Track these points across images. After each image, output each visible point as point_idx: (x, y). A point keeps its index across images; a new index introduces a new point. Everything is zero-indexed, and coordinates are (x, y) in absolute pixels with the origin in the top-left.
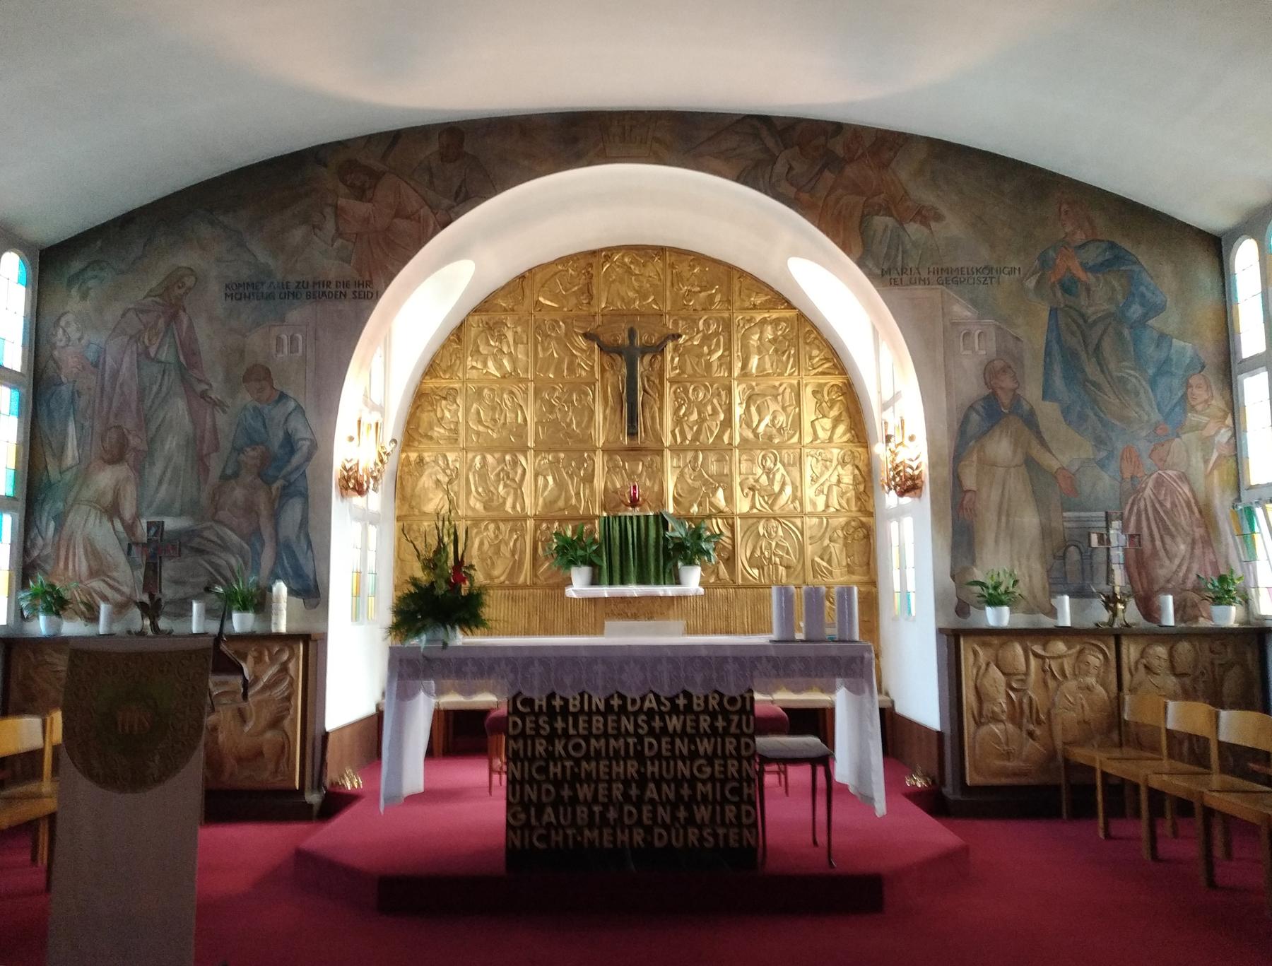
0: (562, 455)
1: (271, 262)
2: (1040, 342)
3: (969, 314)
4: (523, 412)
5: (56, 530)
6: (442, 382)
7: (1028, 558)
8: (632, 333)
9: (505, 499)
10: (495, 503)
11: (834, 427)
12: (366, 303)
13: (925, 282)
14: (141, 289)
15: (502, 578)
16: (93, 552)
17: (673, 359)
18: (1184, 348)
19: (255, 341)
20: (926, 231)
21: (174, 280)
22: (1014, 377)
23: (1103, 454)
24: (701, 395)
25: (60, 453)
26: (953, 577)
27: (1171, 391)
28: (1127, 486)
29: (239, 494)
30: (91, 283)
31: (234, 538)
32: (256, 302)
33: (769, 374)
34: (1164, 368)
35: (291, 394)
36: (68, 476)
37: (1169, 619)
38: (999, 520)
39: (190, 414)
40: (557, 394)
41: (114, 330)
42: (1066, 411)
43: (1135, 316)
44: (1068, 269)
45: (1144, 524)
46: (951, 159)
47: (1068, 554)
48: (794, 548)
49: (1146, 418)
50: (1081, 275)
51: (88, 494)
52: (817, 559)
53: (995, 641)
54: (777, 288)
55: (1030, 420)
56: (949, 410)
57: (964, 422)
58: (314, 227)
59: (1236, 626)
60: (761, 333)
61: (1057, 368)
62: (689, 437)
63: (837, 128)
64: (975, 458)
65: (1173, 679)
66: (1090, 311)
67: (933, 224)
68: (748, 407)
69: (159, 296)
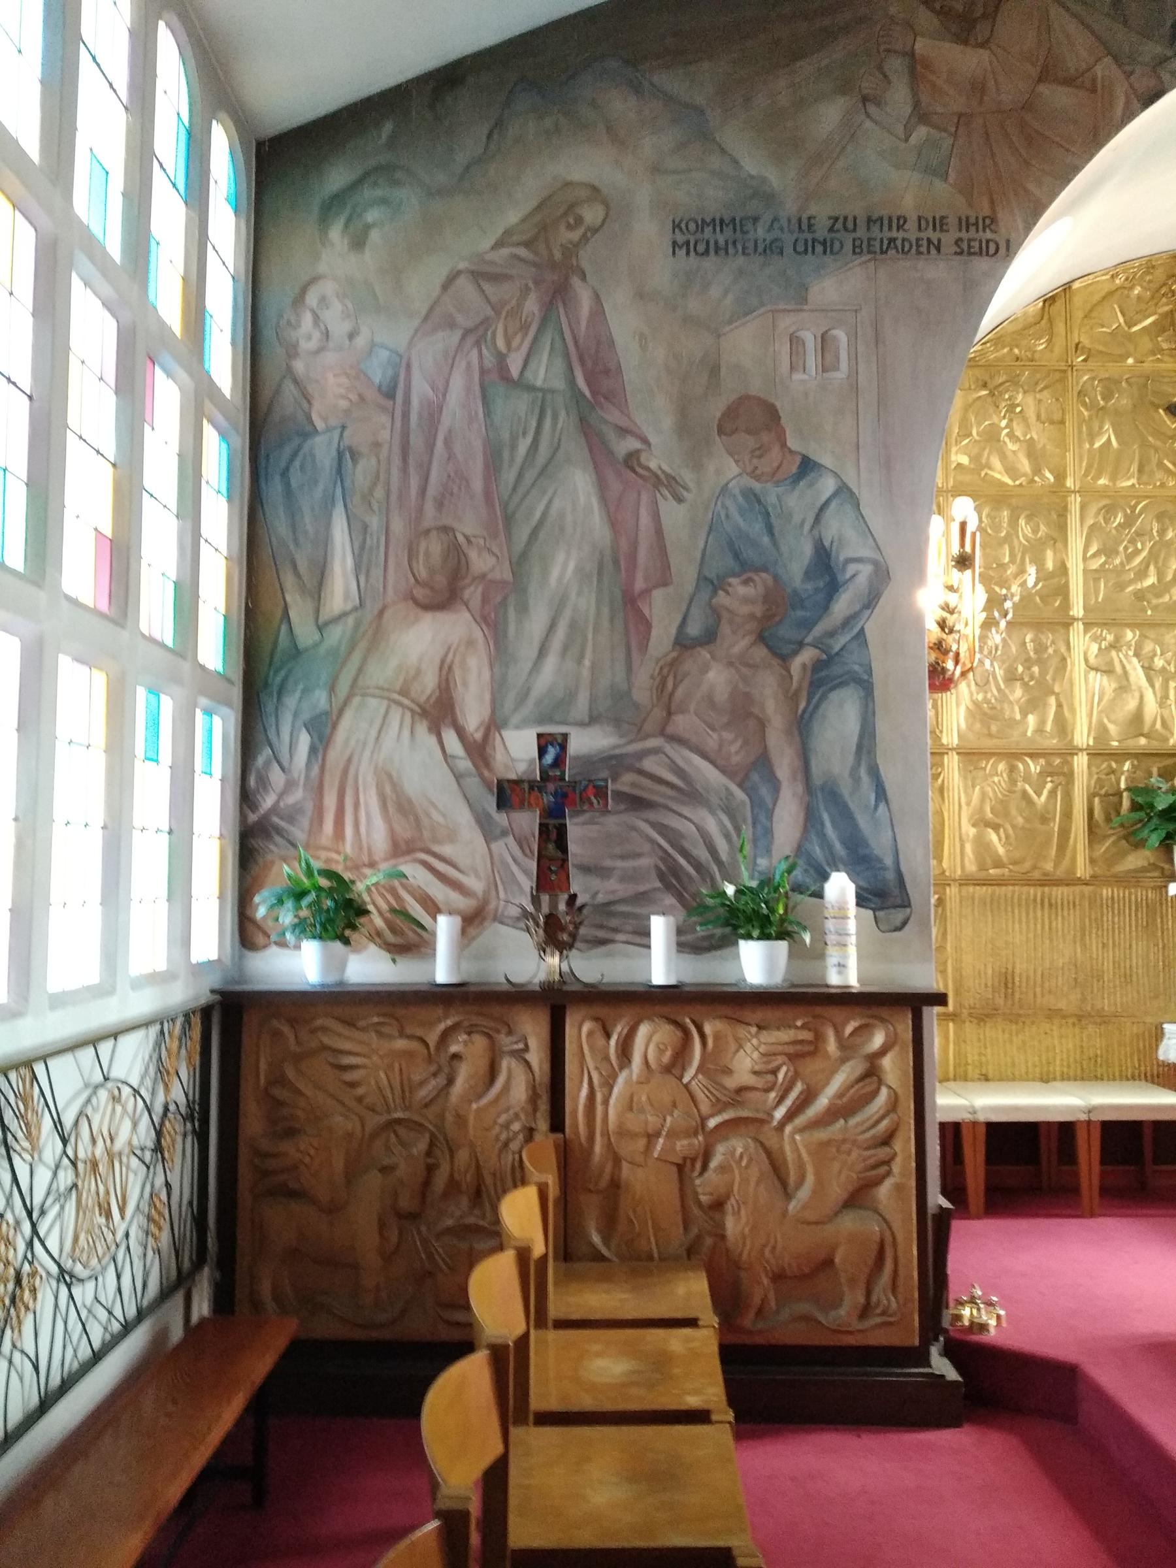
0: (1129, 635)
1: (774, 178)
5: (313, 750)
12: (981, 264)
14: (485, 229)
16: (399, 804)
19: (743, 344)
21: (558, 211)
25: (317, 589)
29: (717, 678)
30: (372, 215)
31: (708, 774)
32: (741, 260)
35: (826, 460)
36: (336, 634)
39: (603, 499)
41: (426, 318)
51: (382, 672)
58: (865, 99)
69: (528, 244)
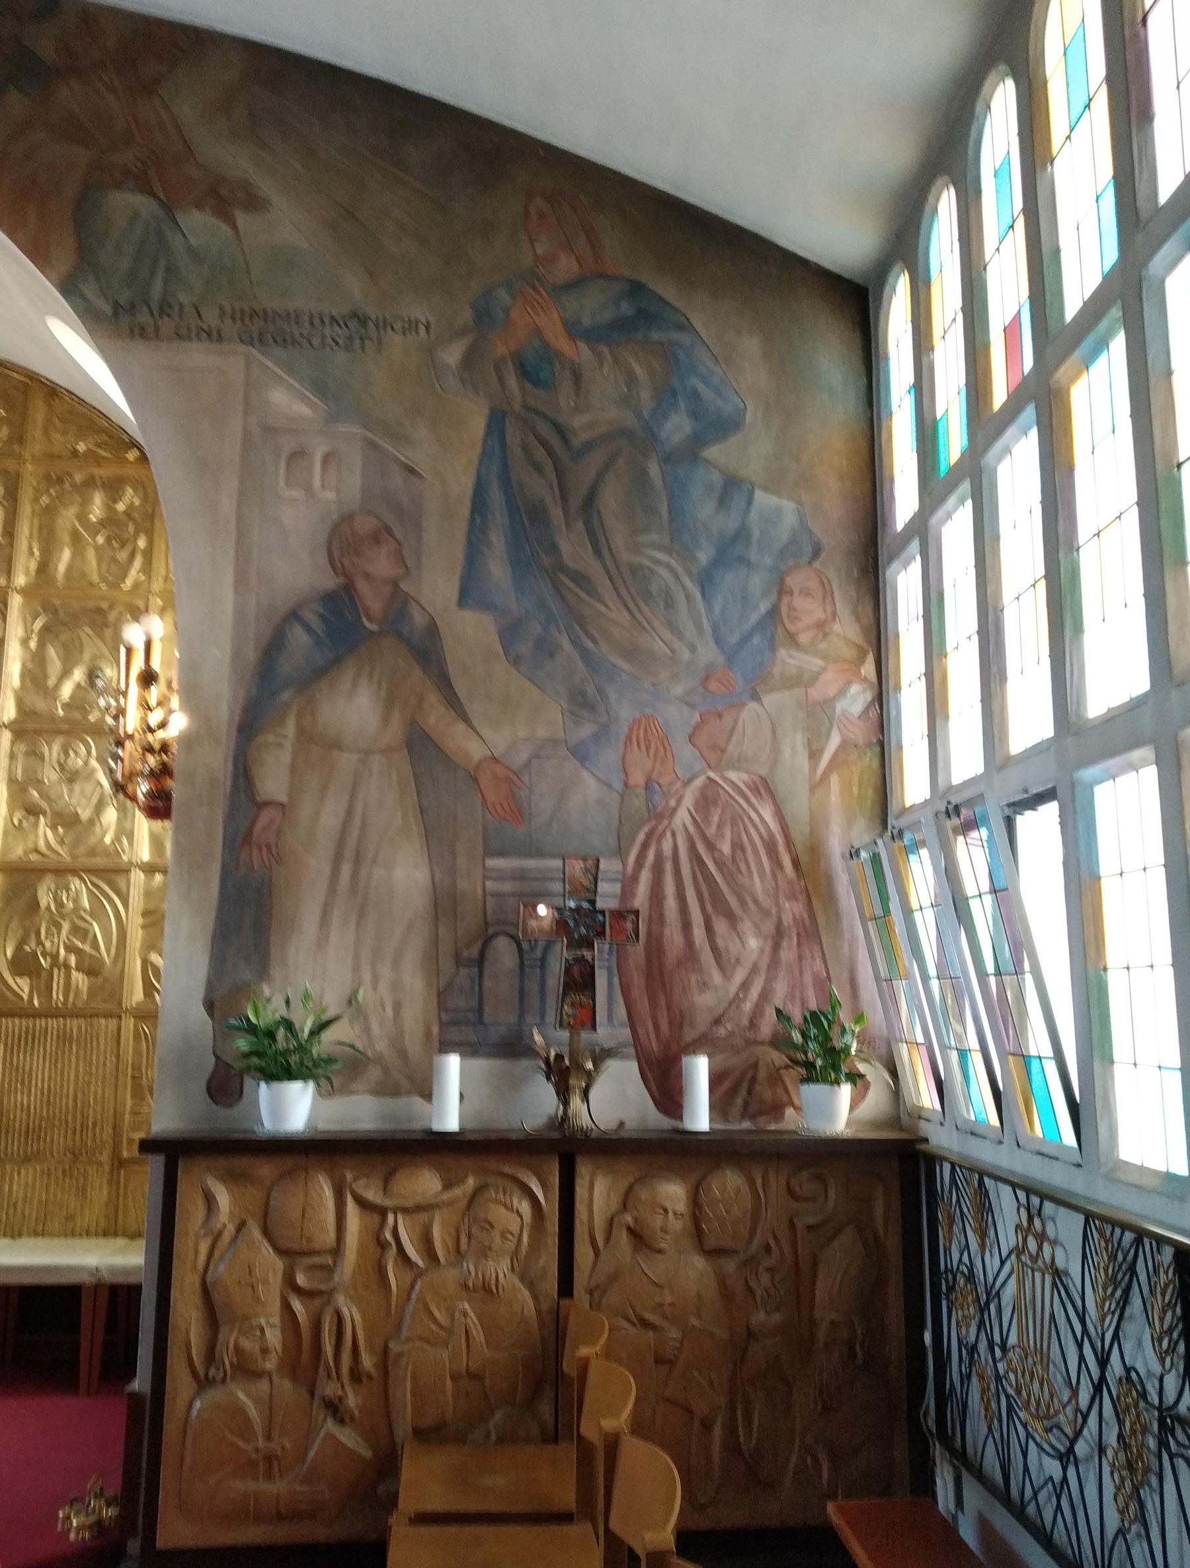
2: (462, 483)
3: (305, 410)
7: (396, 965)
13: (211, 335)
18: (779, 510)
20: (224, 228)
22: (399, 558)
23: (586, 731)
26: (210, 1006)
27: (745, 599)
28: (638, 802)
34: (732, 549)
37: (700, 1117)
42: (510, 633)
43: (677, 439)
44: (538, 332)
45: (670, 889)
47: (490, 954)
49: (686, 655)
50: (563, 344)
53: (265, 1169)
55: (427, 652)
56: (240, 615)
59: (849, 1133)
61: (498, 540)
64: (290, 729)
65: (699, 1263)
66: (579, 421)
67: (241, 217)
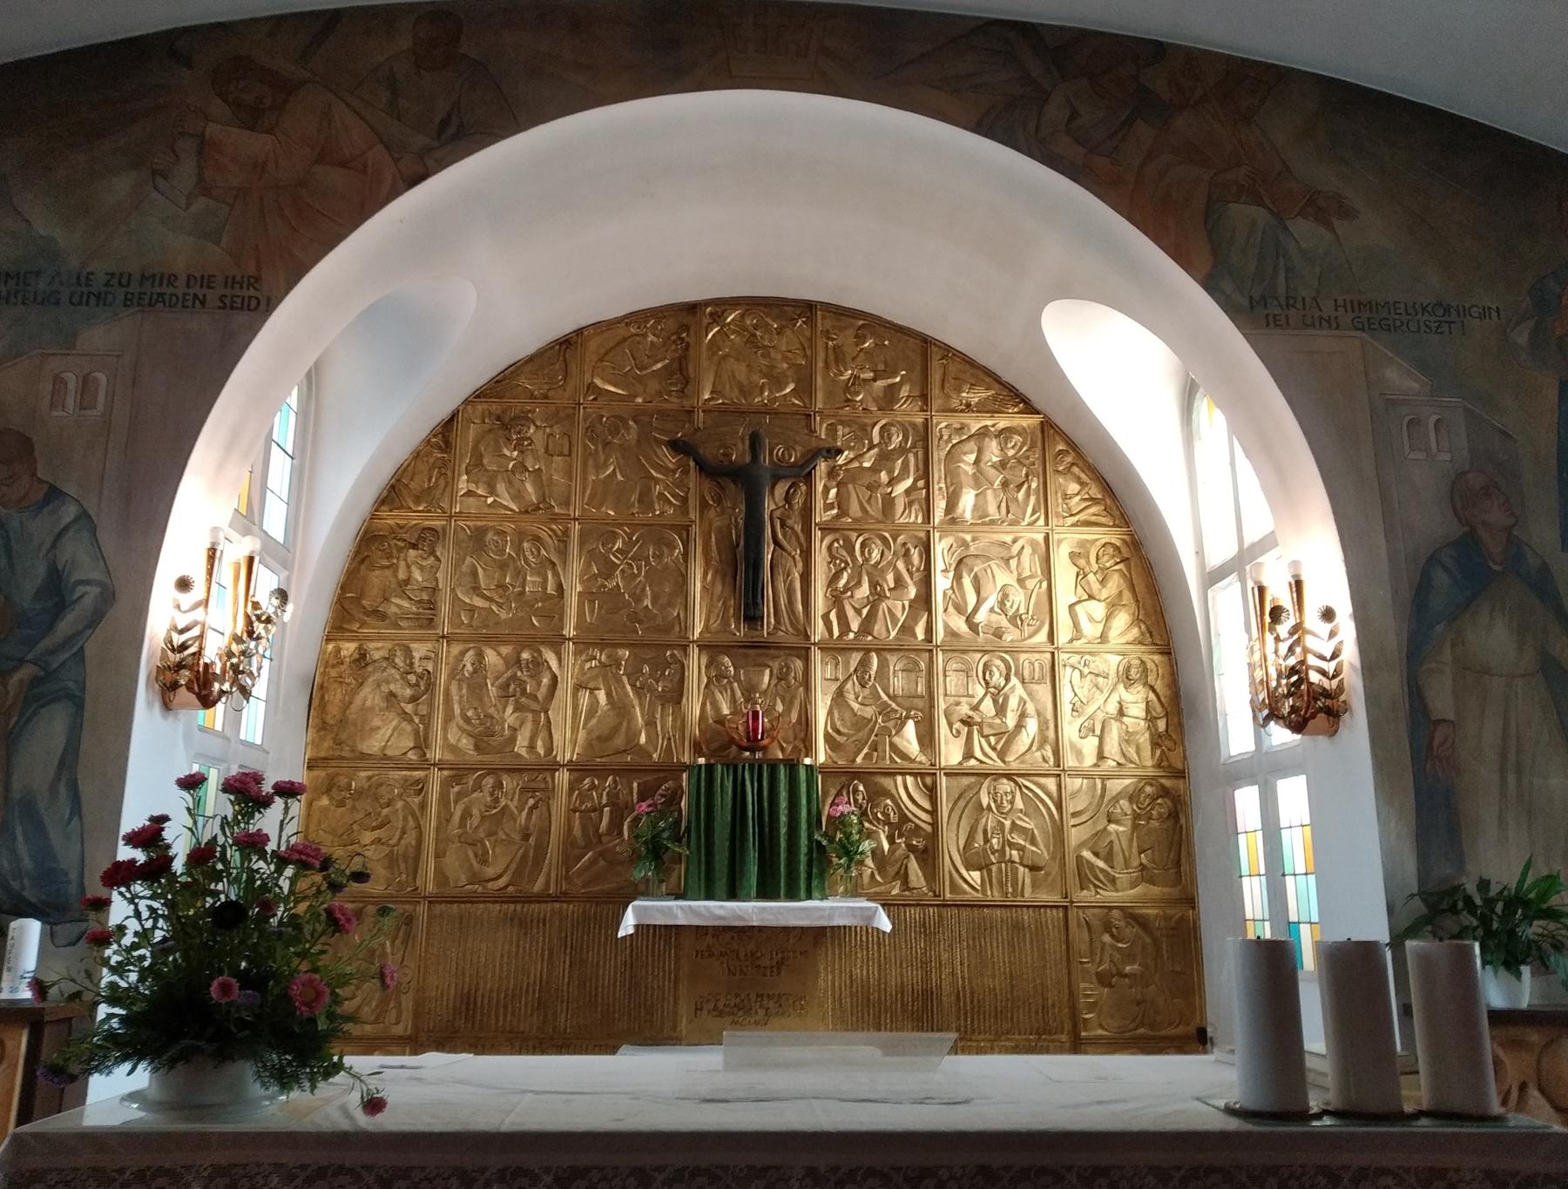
3: (1416, 386)
4: (556, 574)
6: (414, 517)
8: (755, 442)
9: (514, 730)
10: (495, 741)
11: (1109, 617)
12: (241, 318)
13: (1330, 323)
15: (502, 882)
17: (826, 490)
20: (1328, 235)
24: (876, 555)
33: (993, 522)
35: (71, 489)
38: (1503, 781)
40: (619, 544)
46: (1358, 113)
48: (1044, 832)
52: (1087, 854)
54: (1007, 377)
57: (1422, 589)
58: (154, 173)
60: (980, 452)
62: (855, 626)
63: (1156, 51)
64: (1447, 655)
67: (1336, 223)
68: (958, 577)
